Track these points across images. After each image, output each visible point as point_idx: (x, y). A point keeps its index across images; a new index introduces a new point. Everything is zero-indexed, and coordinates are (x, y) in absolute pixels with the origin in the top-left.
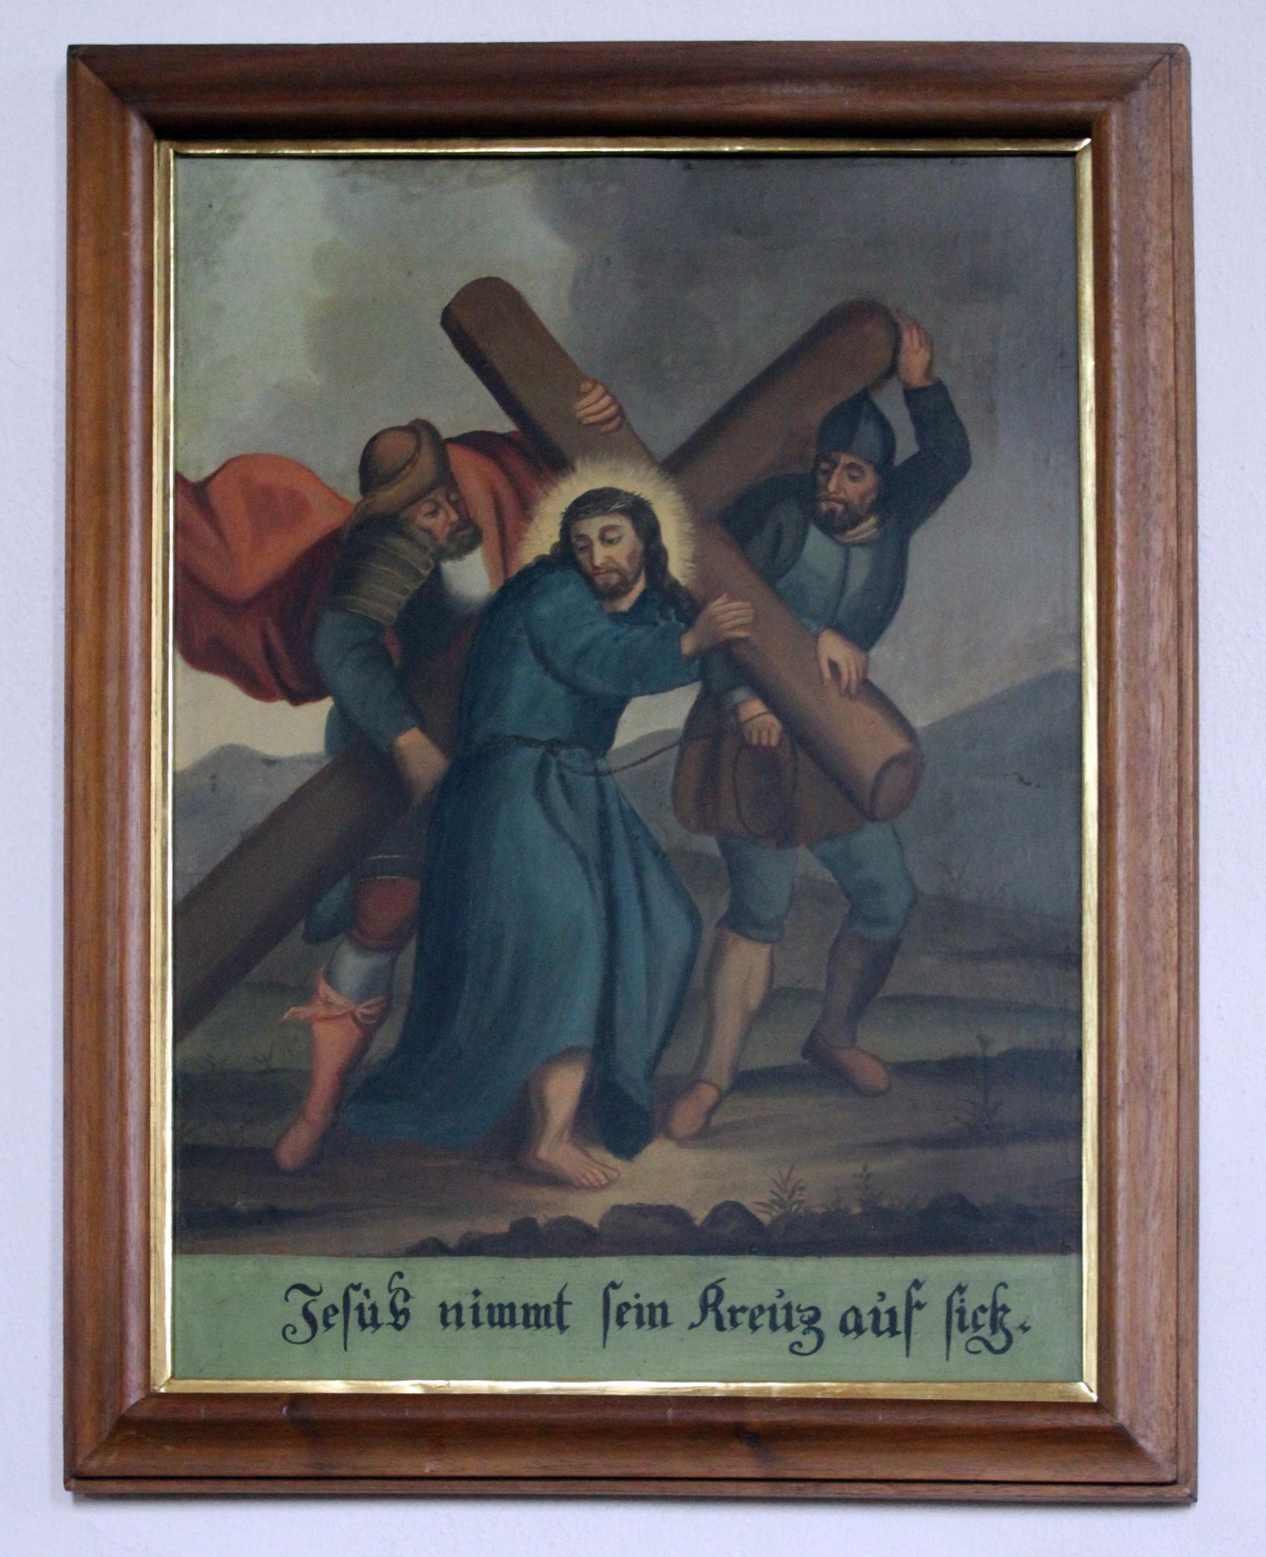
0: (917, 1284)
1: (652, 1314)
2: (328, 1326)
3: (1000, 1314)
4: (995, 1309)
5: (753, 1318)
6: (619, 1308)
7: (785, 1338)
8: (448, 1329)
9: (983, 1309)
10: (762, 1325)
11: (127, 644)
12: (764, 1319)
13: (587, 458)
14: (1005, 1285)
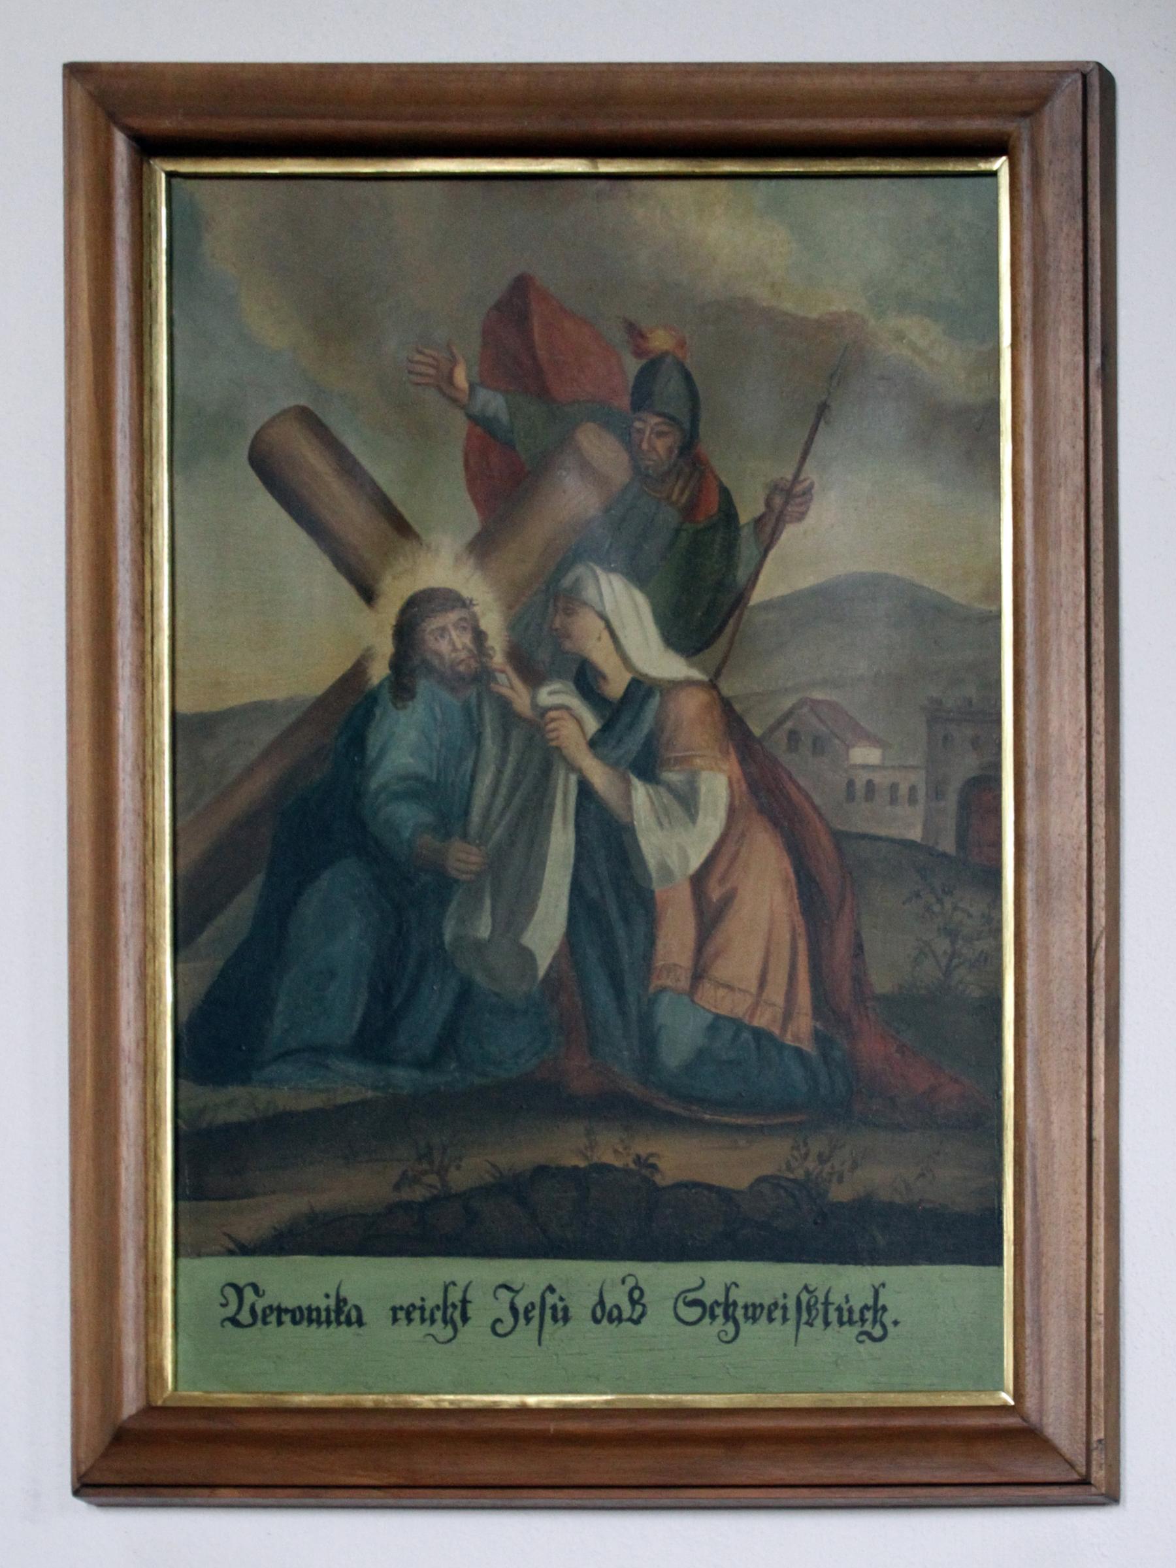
0: (551, 1289)
1: (310, 1314)
3: (880, 1313)
4: (727, 1305)
5: (770, 1313)
6: (264, 1311)
9: (717, 1303)
11: (130, 450)
12: (416, 1315)
14: (737, 1286)
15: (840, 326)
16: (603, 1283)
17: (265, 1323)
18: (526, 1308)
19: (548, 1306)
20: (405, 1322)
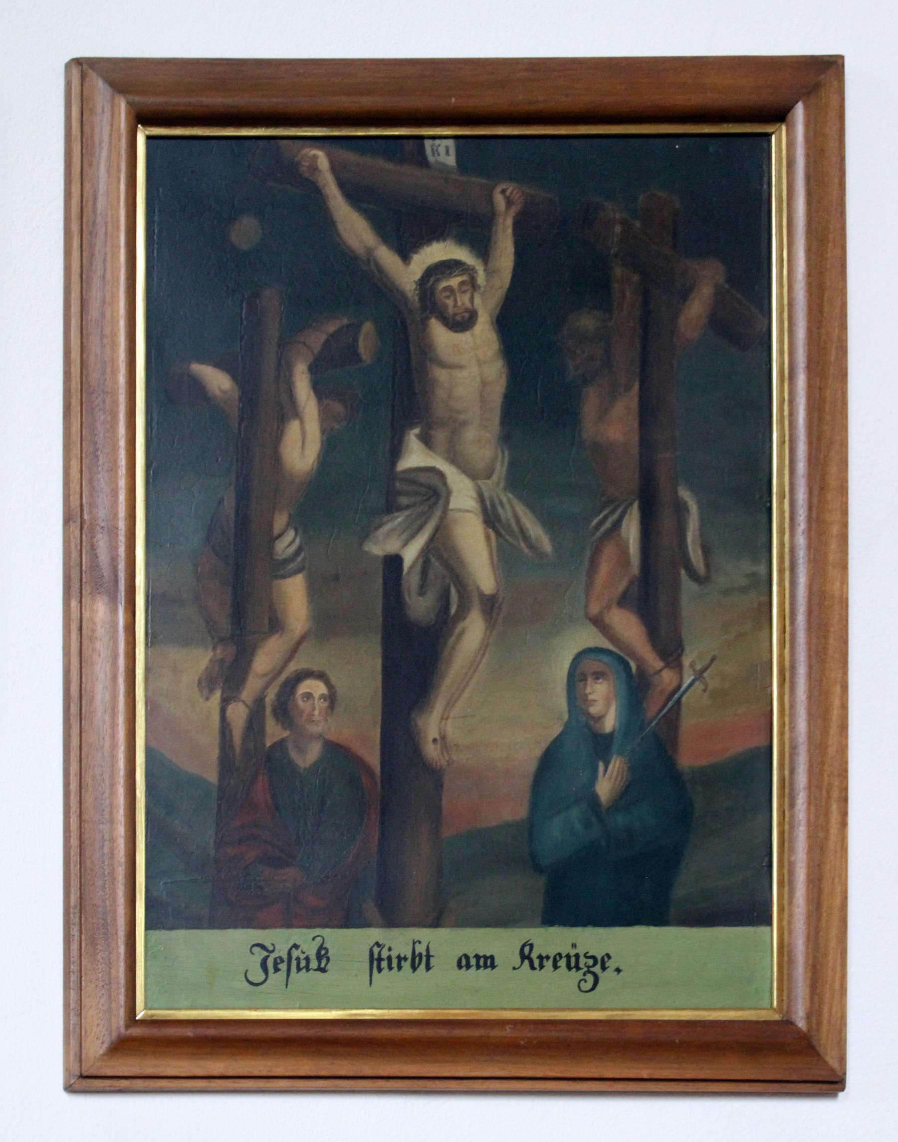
0: (296, 946)
1: (485, 963)
2: (277, 970)
7: (577, 975)
8: (393, 971)
10: (384, 968)
12: (562, 963)
13: (390, 276)
15: (810, 150)
16: (429, 943)
17: (400, 968)
18: (603, 958)
19: (294, 958)
20: (396, 968)
